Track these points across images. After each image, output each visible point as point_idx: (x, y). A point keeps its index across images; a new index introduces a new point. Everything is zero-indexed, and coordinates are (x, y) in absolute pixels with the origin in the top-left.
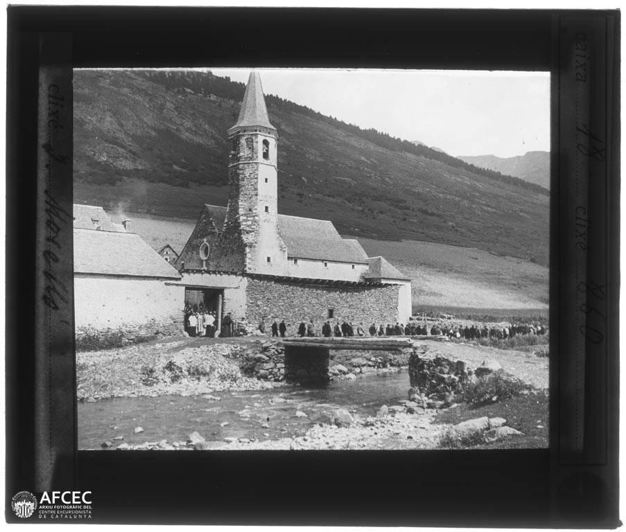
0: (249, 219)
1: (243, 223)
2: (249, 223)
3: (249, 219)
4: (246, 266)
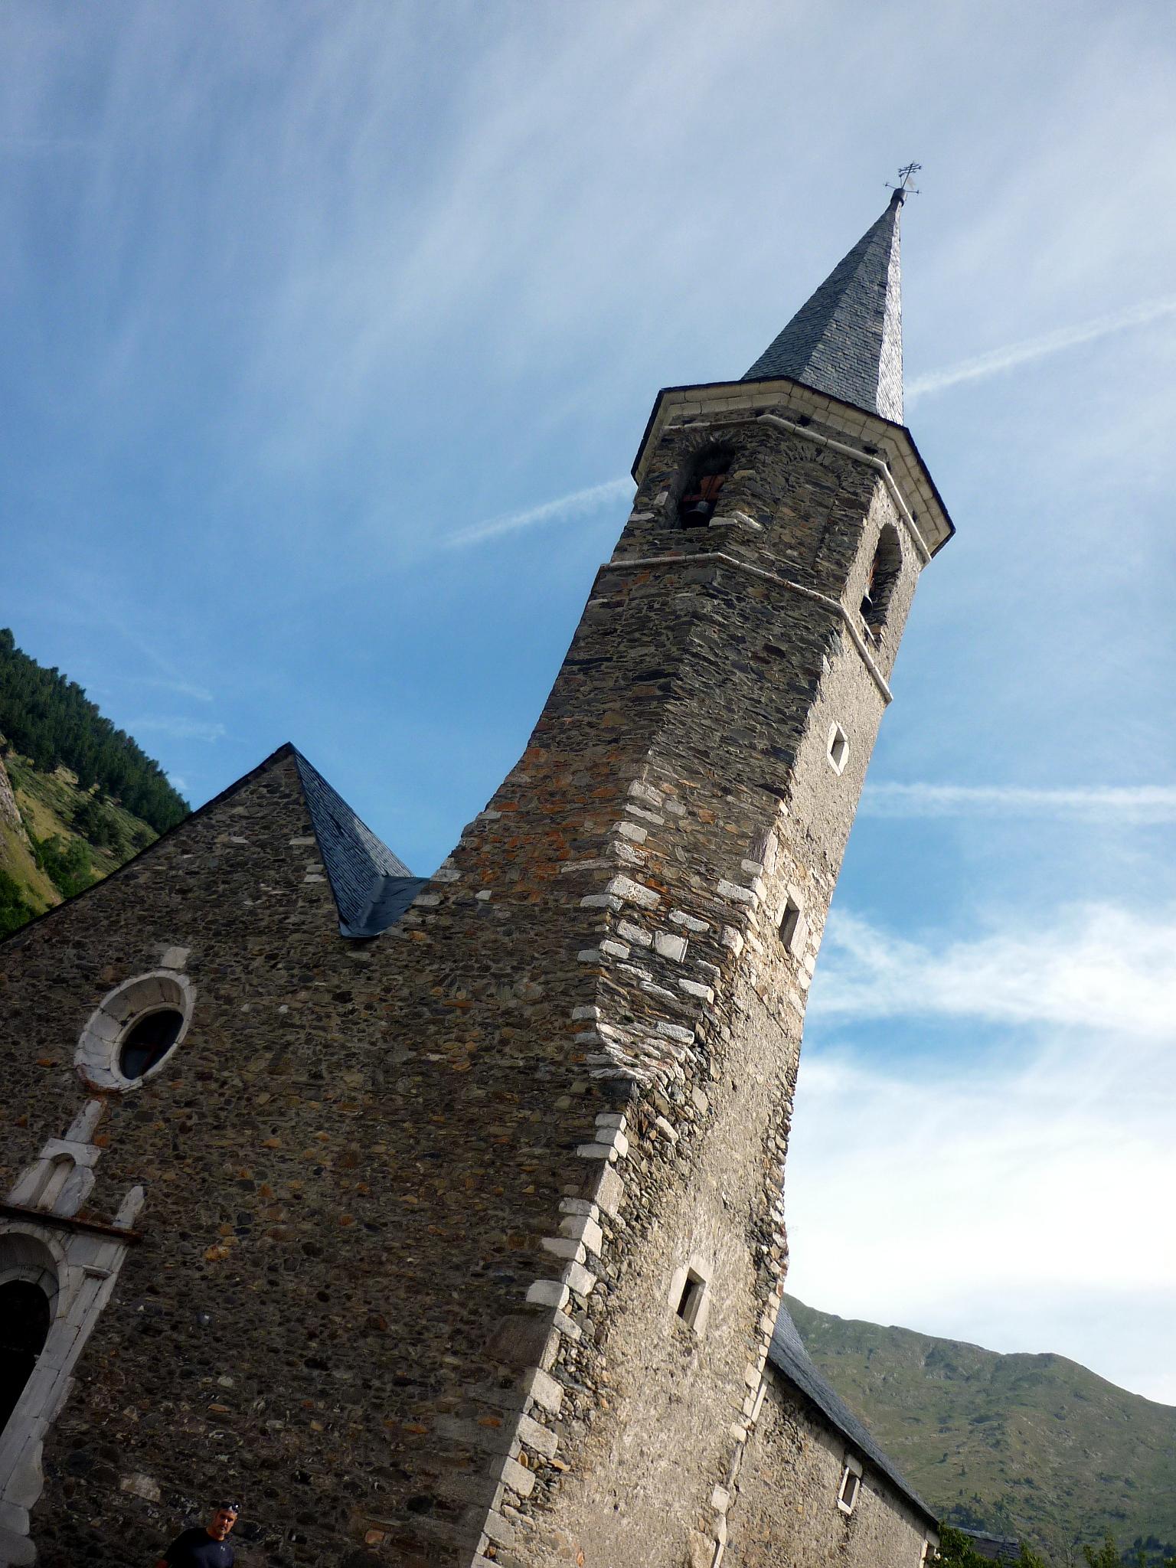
0: (679, 917)
1: (626, 929)
2: (673, 947)
3: (679, 917)
4: (556, 1270)
